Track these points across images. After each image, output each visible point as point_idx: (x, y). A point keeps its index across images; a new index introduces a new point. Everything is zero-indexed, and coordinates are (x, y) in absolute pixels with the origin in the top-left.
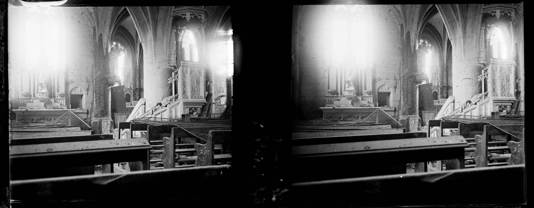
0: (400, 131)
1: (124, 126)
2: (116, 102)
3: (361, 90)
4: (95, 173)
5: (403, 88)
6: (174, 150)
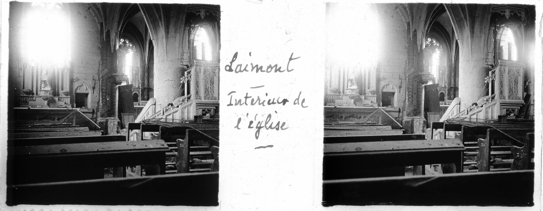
0: (99, 134)
1: (437, 126)
2: (430, 101)
3: (58, 90)
4: (406, 174)
5: (102, 89)
6: (490, 153)
